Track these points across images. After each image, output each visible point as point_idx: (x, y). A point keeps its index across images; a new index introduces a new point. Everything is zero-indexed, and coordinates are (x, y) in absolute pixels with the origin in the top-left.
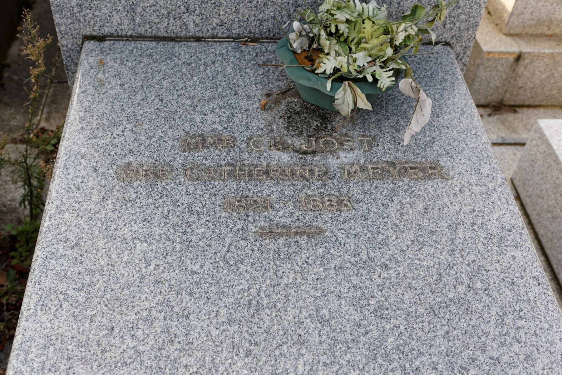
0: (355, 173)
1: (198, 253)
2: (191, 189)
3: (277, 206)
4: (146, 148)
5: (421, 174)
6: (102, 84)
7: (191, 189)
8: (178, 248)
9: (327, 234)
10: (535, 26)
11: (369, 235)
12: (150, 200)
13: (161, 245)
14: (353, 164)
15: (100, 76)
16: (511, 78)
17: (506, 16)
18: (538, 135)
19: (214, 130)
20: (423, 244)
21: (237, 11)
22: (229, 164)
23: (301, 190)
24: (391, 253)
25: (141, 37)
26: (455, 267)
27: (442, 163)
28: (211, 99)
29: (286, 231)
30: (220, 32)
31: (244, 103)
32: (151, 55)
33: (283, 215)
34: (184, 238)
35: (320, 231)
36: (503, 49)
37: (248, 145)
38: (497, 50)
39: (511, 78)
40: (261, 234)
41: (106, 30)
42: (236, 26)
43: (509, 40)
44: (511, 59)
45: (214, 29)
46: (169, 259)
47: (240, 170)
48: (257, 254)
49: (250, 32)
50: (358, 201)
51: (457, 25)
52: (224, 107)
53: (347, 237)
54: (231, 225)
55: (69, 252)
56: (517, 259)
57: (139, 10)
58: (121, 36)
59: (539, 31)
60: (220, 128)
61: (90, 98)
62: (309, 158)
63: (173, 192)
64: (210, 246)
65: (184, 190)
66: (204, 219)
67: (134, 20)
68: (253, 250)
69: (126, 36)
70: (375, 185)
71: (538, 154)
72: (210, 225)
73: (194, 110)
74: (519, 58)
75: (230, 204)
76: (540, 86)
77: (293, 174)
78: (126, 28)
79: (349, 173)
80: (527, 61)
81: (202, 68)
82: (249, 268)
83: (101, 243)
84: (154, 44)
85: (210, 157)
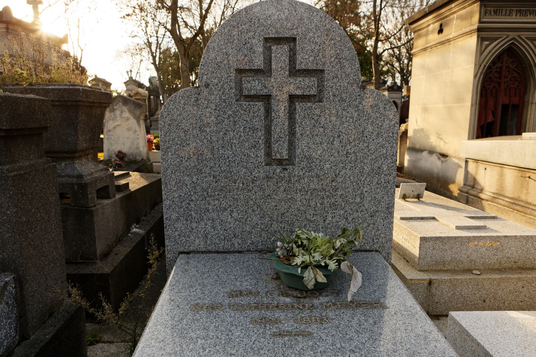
0: (330, 306)
1: (235, 344)
2: (233, 315)
3: (283, 322)
4: (208, 296)
5: (370, 306)
6: (186, 270)
7: (233, 315)
8: (223, 342)
9: (315, 335)
10: (435, 265)
11: (341, 335)
12: (208, 320)
13: (213, 341)
14: (328, 302)
15: (186, 267)
16: (429, 296)
17: (417, 260)
18: (452, 322)
19: (247, 289)
20: (376, 339)
21: (261, 236)
22: (255, 303)
23: (297, 315)
24: (355, 344)
25: (210, 252)
26: (398, 352)
27: (381, 301)
28: (245, 276)
29: (289, 334)
30: (252, 248)
31: (264, 277)
32: (214, 259)
33: (287, 326)
34: (227, 337)
35: (310, 334)
36: (419, 277)
37: (266, 295)
38: (416, 278)
39: (429, 296)
40: (274, 335)
41: (192, 248)
42: (260, 244)
43: (422, 273)
44: (426, 283)
45: (248, 246)
46: (218, 348)
47: (262, 305)
48: (271, 345)
49: (268, 248)
50: (332, 319)
51: (380, 240)
52: (253, 279)
53: (327, 336)
54: (256, 331)
55: (158, 344)
56: (438, 347)
57: (209, 236)
58: (199, 252)
59: (439, 268)
60: (251, 288)
61: (179, 276)
62: (302, 300)
63: (222, 316)
64: (243, 341)
65: (228, 315)
66: (239, 328)
67: (206, 242)
68: (269, 343)
69: (201, 252)
70: (342, 311)
71: (456, 334)
72: (243, 331)
73: (236, 280)
74: (430, 283)
75: (255, 321)
76: (449, 301)
77: (293, 307)
78: (202, 247)
79: (326, 306)
80: (436, 285)
81: (241, 263)
82: (266, 352)
83: (177, 340)
84: (216, 255)
85: (244, 300)
